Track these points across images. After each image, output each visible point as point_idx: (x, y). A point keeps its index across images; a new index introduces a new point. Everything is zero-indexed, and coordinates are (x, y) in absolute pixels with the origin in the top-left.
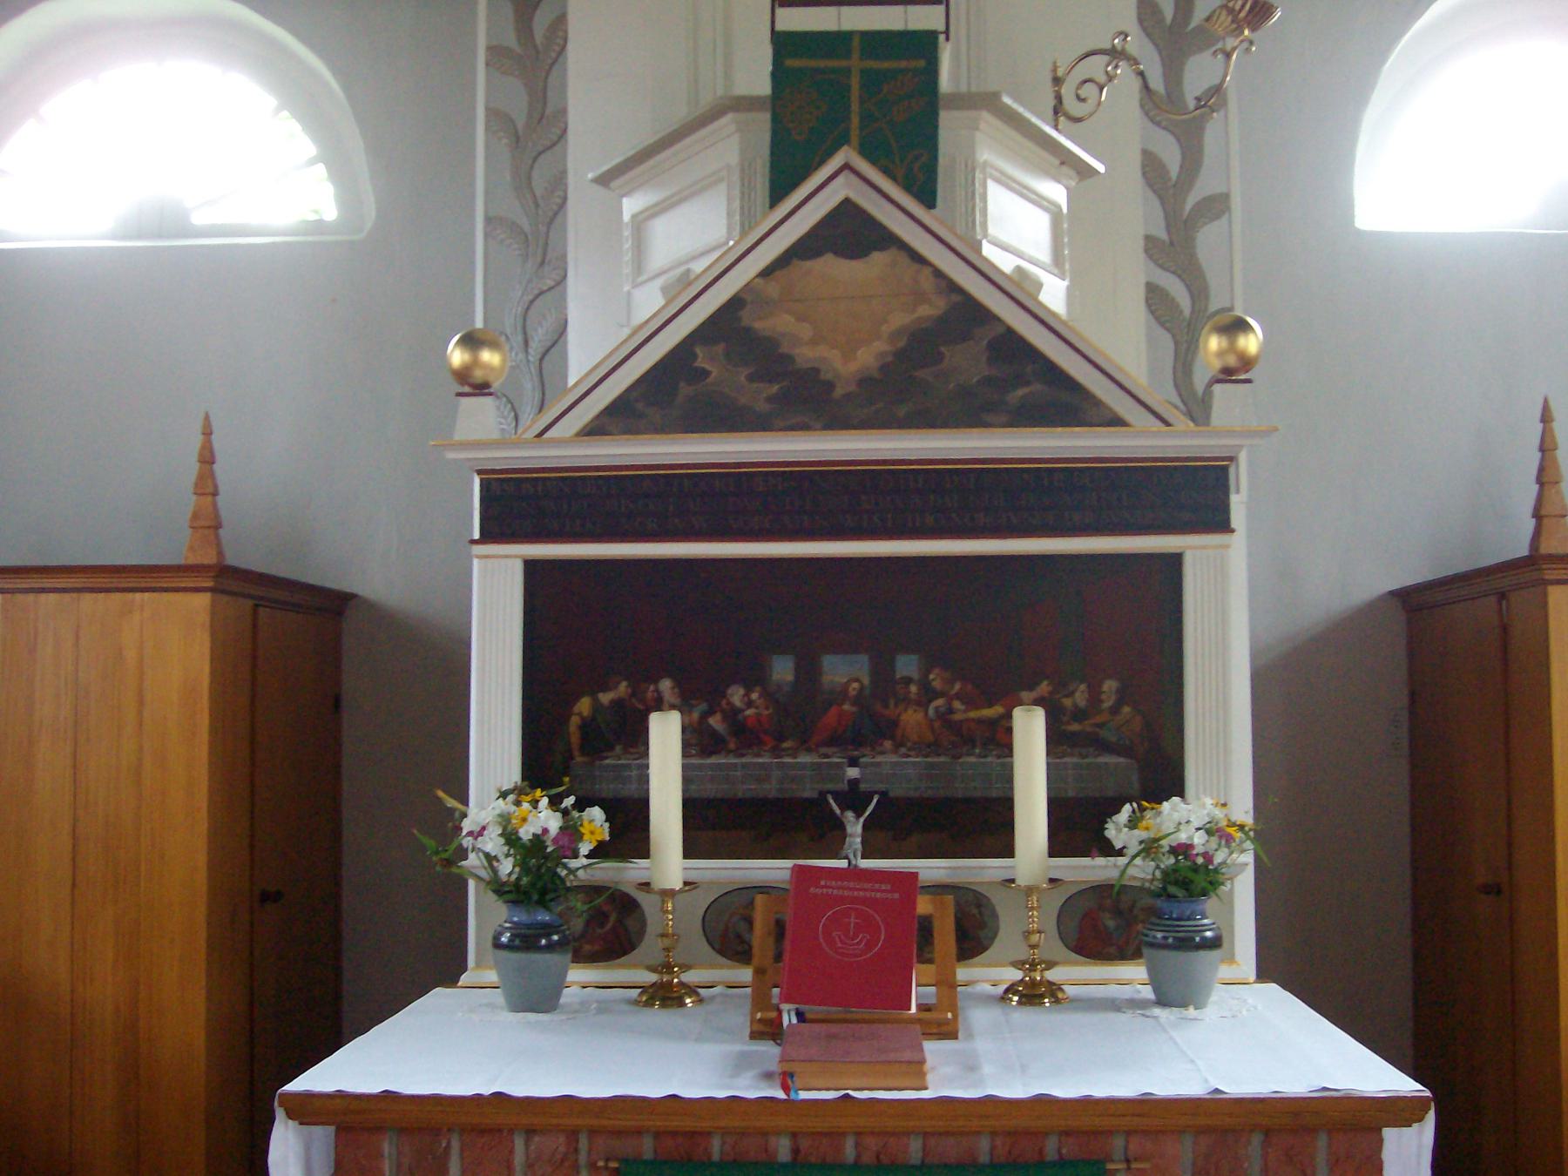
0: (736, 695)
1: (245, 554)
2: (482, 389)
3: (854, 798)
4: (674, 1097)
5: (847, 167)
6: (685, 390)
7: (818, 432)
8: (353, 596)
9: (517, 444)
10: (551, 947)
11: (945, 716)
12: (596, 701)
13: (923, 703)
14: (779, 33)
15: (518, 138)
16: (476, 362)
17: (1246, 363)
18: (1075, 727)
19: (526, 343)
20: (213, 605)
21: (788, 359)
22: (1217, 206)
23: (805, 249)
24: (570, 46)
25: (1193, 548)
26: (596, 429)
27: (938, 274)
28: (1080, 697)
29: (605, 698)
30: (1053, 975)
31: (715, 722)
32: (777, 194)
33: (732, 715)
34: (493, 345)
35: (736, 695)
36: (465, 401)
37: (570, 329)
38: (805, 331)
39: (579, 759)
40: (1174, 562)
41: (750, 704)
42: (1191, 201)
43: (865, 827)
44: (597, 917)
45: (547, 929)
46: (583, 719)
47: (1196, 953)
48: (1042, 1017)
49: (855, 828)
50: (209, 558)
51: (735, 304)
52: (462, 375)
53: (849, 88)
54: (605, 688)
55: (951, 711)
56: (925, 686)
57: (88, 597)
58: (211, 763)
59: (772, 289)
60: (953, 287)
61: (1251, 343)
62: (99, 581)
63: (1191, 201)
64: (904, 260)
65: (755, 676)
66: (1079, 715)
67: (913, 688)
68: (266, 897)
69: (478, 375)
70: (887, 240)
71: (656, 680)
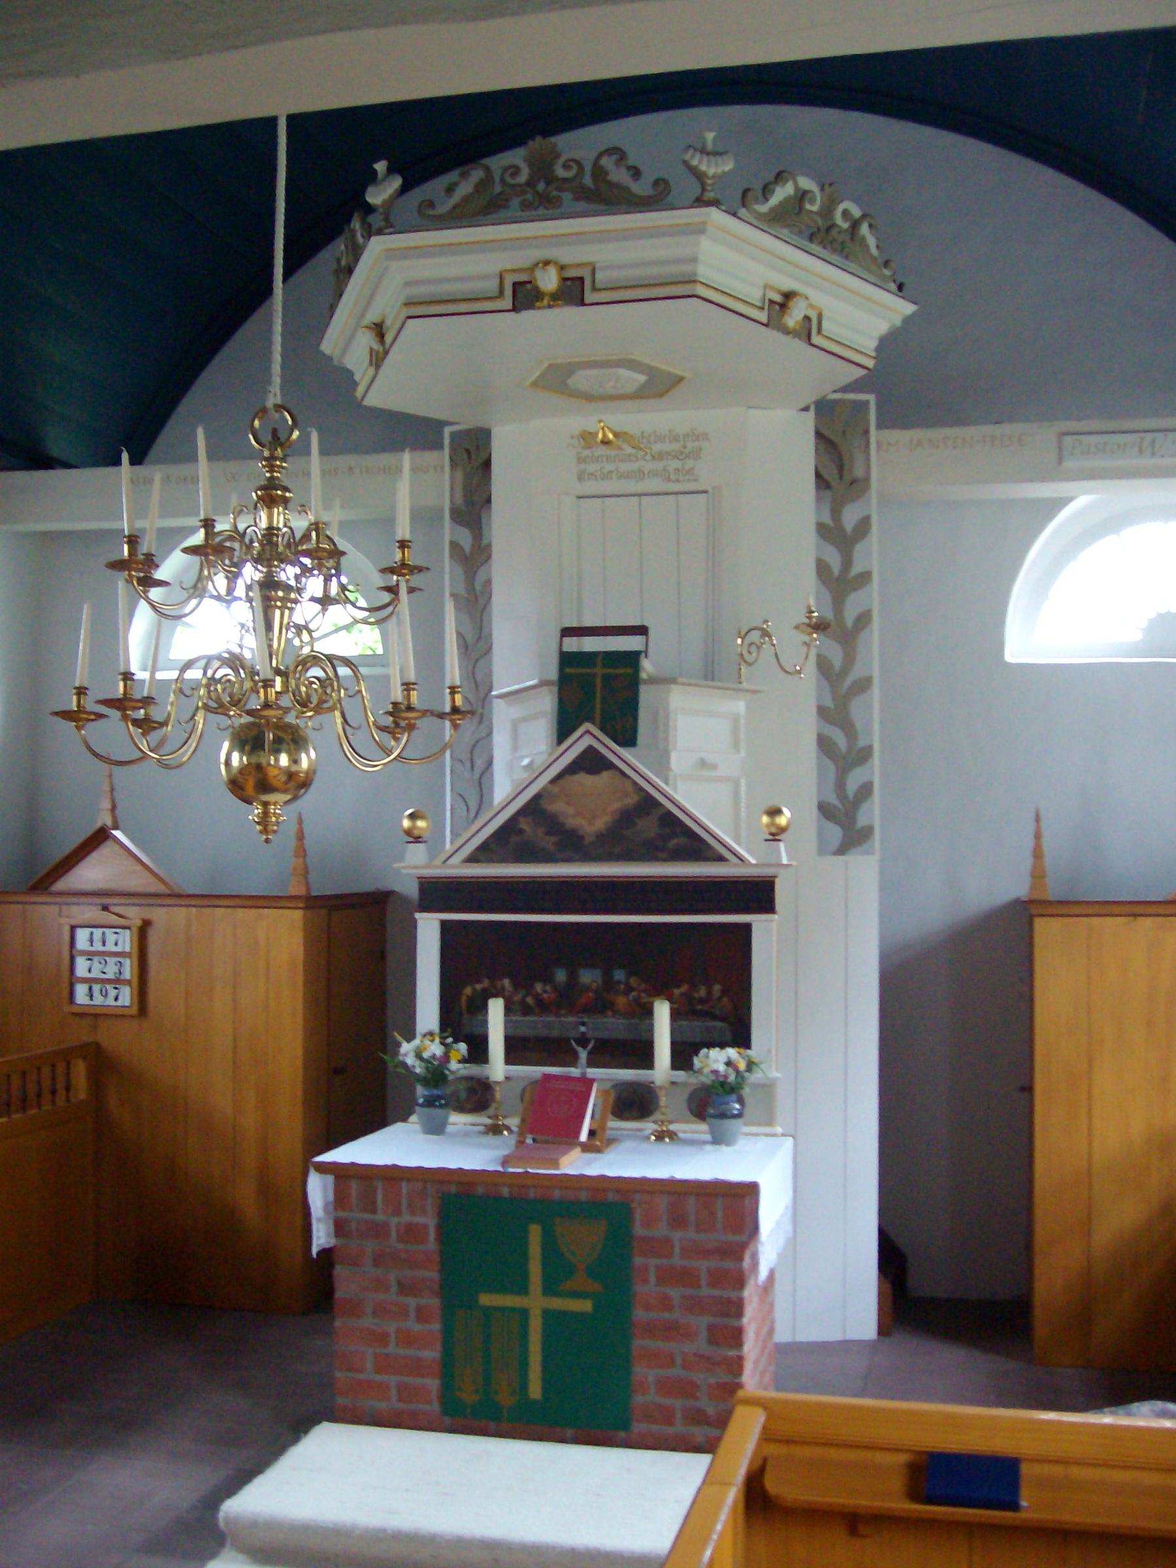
0: (539, 987)
1: (320, 888)
2: (417, 839)
3: (583, 1041)
4: (461, 1169)
5: (588, 732)
6: (514, 839)
7: (577, 863)
8: (394, 891)
9: (436, 867)
10: (441, 1106)
11: (637, 1001)
12: (474, 989)
13: (626, 994)
14: (563, 652)
15: (467, 648)
16: (414, 827)
17: (783, 830)
18: (699, 1007)
19: (472, 767)
20: (304, 916)
21: (563, 825)
22: (864, 685)
23: (572, 769)
24: (494, 598)
25: (757, 921)
26: (472, 859)
27: (635, 783)
28: (702, 992)
29: (478, 987)
30: (672, 1127)
31: (530, 1000)
32: (560, 741)
33: (537, 997)
34: (422, 817)
35: (539, 987)
36: (410, 845)
37: (495, 761)
38: (570, 810)
39: (466, 1016)
40: (747, 927)
41: (545, 992)
42: (849, 681)
43: (589, 1053)
44: (471, 1091)
45: (439, 1097)
46: (468, 996)
47: (721, 1121)
48: (667, 1145)
49: (583, 1055)
50: (301, 891)
51: (537, 797)
52: (408, 832)
53: (594, 686)
54: (479, 982)
55: (640, 997)
56: (627, 984)
57: (241, 911)
58: (305, 1000)
59: (555, 789)
60: (641, 789)
61: (782, 821)
62: (250, 903)
63: (849, 681)
64: (618, 773)
65: (548, 979)
66: (701, 1001)
67: (622, 987)
68: (337, 1071)
69: (416, 833)
70: (611, 766)
71: (501, 979)
